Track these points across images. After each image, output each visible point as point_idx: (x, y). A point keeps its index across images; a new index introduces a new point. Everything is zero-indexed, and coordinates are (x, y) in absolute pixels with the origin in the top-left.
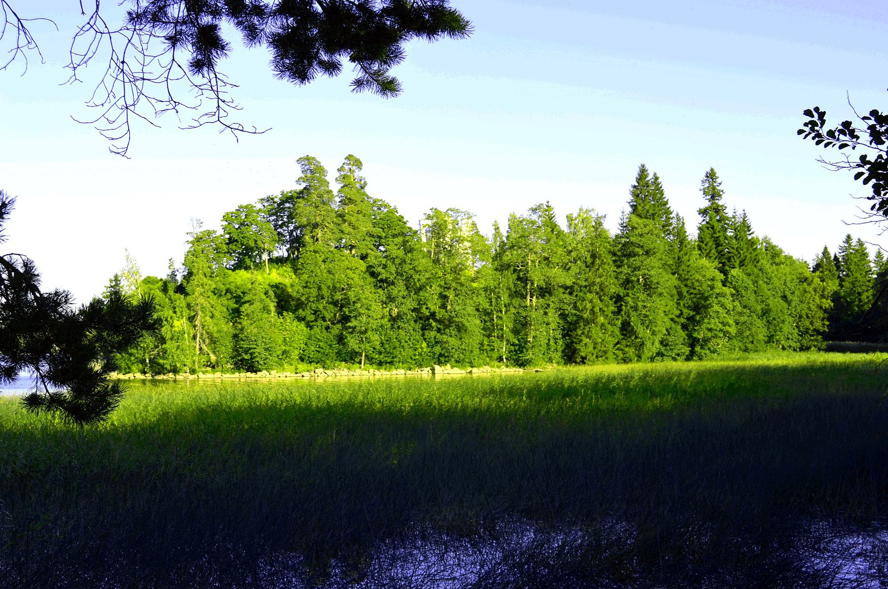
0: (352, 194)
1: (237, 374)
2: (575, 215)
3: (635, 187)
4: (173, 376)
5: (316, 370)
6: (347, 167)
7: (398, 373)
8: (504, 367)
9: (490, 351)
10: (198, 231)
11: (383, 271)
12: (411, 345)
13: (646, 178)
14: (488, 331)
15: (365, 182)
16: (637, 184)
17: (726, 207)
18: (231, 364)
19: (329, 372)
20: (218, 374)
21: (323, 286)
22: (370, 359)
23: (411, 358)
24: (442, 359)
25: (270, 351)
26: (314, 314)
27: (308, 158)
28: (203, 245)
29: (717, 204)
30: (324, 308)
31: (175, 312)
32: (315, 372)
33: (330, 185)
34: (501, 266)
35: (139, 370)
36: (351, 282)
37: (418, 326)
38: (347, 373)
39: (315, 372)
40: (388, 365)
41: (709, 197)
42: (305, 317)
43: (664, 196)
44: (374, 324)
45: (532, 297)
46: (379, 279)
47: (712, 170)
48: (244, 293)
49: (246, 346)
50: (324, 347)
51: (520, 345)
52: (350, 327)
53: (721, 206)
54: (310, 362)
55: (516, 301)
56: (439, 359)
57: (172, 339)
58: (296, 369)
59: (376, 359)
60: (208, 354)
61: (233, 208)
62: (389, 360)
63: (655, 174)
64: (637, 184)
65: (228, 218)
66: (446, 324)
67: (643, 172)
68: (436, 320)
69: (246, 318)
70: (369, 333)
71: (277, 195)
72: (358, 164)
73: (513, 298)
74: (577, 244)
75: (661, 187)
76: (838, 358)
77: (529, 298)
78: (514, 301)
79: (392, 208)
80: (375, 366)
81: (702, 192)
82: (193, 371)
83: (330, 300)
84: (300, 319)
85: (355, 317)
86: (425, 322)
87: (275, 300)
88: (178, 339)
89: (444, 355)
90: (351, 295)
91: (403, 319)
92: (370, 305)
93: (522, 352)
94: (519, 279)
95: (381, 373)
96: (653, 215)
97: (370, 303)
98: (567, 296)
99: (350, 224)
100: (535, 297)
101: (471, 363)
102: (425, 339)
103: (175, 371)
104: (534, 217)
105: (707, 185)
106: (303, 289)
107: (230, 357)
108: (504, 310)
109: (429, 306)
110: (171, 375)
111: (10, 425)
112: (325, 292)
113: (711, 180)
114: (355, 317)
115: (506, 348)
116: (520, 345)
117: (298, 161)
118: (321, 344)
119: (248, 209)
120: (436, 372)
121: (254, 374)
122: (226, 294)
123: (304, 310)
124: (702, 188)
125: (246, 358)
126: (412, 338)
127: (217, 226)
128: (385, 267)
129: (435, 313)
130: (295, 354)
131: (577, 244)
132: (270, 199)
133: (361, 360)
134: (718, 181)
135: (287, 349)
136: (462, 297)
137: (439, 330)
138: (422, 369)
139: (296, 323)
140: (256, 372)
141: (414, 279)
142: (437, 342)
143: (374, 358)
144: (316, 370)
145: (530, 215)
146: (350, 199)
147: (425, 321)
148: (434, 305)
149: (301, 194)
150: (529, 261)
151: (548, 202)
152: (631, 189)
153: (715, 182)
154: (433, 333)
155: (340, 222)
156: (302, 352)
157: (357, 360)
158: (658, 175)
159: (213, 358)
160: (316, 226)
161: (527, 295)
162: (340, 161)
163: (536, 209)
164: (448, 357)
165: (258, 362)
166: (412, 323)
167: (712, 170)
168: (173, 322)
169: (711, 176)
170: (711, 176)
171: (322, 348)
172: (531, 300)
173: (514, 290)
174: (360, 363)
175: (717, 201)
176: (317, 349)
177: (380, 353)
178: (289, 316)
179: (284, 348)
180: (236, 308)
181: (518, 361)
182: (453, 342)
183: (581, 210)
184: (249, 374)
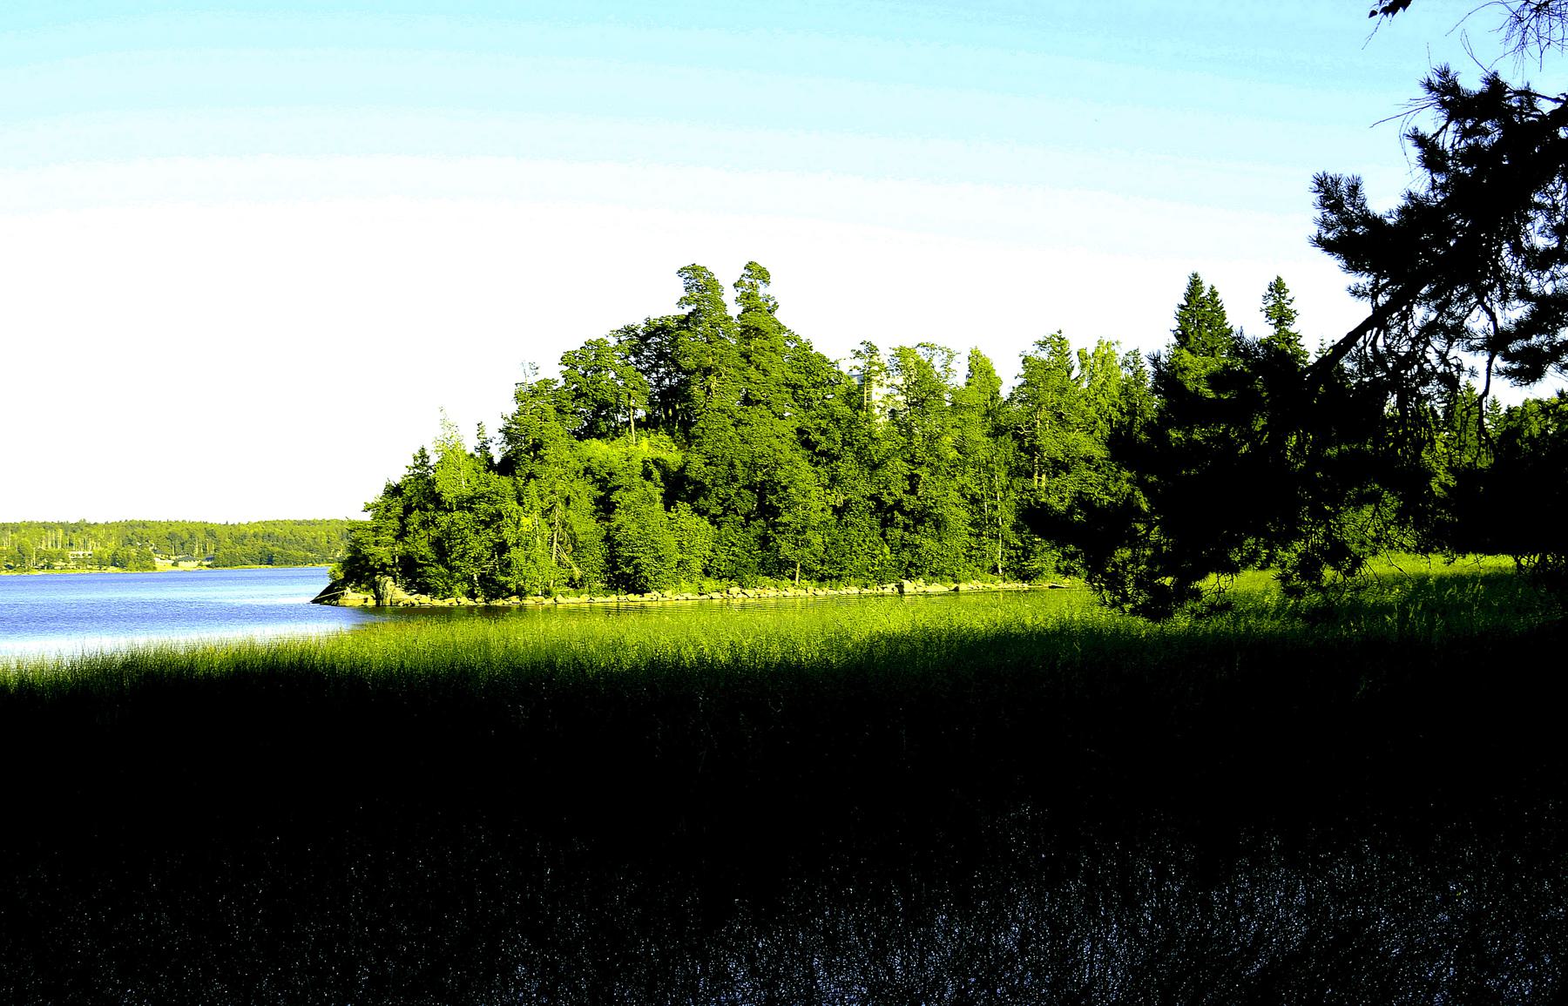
0: (754, 319)
1: (613, 597)
2: (1089, 353)
3: (1182, 307)
4: (518, 601)
5: (731, 590)
6: (747, 281)
7: (849, 591)
8: (1000, 581)
9: (980, 558)
10: (533, 380)
11: (823, 438)
12: (867, 550)
13: (1200, 294)
14: (978, 525)
15: (775, 303)
16: (1185, 303)
17: (1301, 336)
18: (602, 582)
19: (750, 592)
20: (585, 598)
21: (737, 462)
22: (808, 572)
23: (868, 570)
24: (912, 571)
25: (663, 561)
26: (721, 505)
27: (694, 268)
28: (538, 402)
29: (1286, 331)
30: (738, 494)
31: (521, 504)
32: (728, 592)
33: (727, 308)
34: (997, 429)
35: (463, 593)
36: (779, 455)
37: (875, 522)
38: (775, 594)
39: (728, 592)
40: (834, 580)
41: (1274, 321)
42: (708, 509)
43: (1226, 321)
44: (815, 519)
45: (1040, 475)
46: (817, 451)
47: (1279, 279)
48: (610, 474)
49: (626, 554)
50: (740, 554)
51: (1024, 549)
52: (781, 524)
53: (1294, 335)
54: (720, 578)
55: (1018, 483)
56: (907, 571)
57: (517, 545)
58: (701, 588)
59: (817, 572)
60: (570, 568)
61: (576, 345)
62: (835, 573)
63: (1213, 287)
64: (1185, 303)
65: (569, 360)
66: (919, 518)
67: (1195, 283)
68: (903, 512)
69: (624, 512)
70: (809, 534)
71: (639, 322)
72: (764, 275)
73: (1013, 478)
74: (1096, 395)
75: (1221, 308)
76: (1468, 563)
77: (1036, 477)
78: (1015, 482)
79: (803, 342)
80: (815, 583)
81: (1264, 314)
82: (547, 594)
83: (747, 483)
84: (701, 512)
85: (788, 508)
86: (885, 515)
87: (662, 484)
88: (527, 544)
89: (915, 565)
90: (780, 474)
91: (852, 510)
92: (809, 491)
93: (1027, 559)
94: (1021, 448)
95: (824, 593)
96: (1213, 349)
97: (809, 488)
98: (1094, 474)
99: (757, 368)
100: (1044, 476)
101: (953, 575)
102: (887, 541)
103: (521, 593)
104: (1044, 355)
105: (1271, 303)
106: (705, 466)
107: (602, 571)
108: (1000, 494)
109: (893, 490)
110: (515, 599)
111: (633, 655)
112: (740, 471)
113: (1277, 295)
114: (788, 508)
115: (1003, 553)
116: (1024, 549)
117: (679, 272)
118: (737, 550)
119: (596, 347)
120: (905, 590)
121: (638, 596)
122: (584, 475)
123: (706, 499)
124: (1264, 307)
125: (628, 571)
126: (867, 539)
127: (553, 371)
128: (824, 432)
129: (901, 501)
130: (697, 565)
131: (1096, 395)
132: (629, 330)
133: (795, 573)
134: (1289, 296)
135: (686, 557)
136: (941, 478)
137: (906, 528)
138: (884, 586)
139: (695, 516)
140: (642, 593)
141: (870, 451)
142: (904, 546)
143: (814, 570)
144: (731, 590)
145: (1036, 352)
146: (757, 329)
147: (884, 512)
148: (898, 490)
149: (684, 322)
150: (1038, 421)
151: (1060, 332)
152: (1178, 310)
153: (1284, 298)
154: (898, 532)
155: (744, 365)
156: (708, 563)
157: (789, 572)
158: (1216, 289)
159: (577, 573)
160: (708, 371)
161: (1034, 472)
162: (737, 272)
163: (1045, 343)
164: (921, 567)
165: (646, 578)
166: (867, 516)
167: (1279, 279)
168: (519, 519)
169: (1278, 288)
170: (1278, 288)
171: (737, 556)
172: (1039, 480)
173: (1014, 465)
174: (793, 578)
175: (1287, 327)
176: (731, 558)
177: (823, 562)
178: (684, 507)
179: (679, 556)
180: (601, 497)
181: (1021, 573)
182: (929, 544)
183: (1100, 342)
184: (631, 596)
